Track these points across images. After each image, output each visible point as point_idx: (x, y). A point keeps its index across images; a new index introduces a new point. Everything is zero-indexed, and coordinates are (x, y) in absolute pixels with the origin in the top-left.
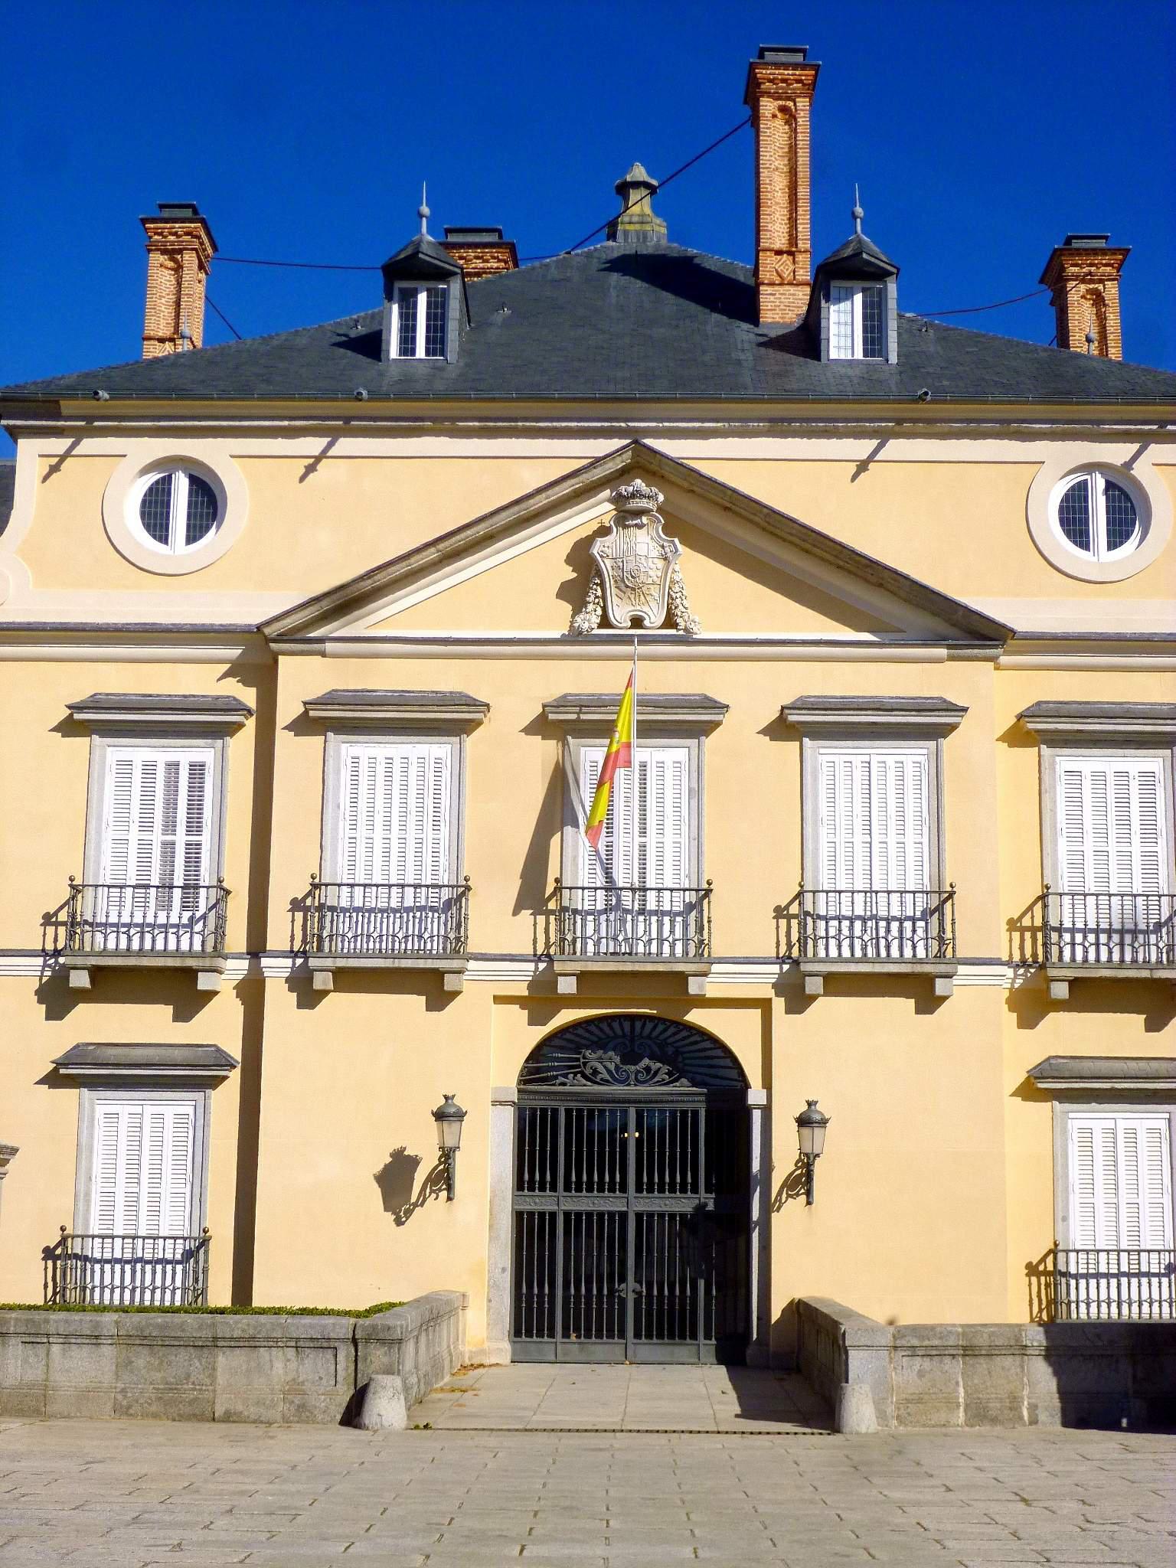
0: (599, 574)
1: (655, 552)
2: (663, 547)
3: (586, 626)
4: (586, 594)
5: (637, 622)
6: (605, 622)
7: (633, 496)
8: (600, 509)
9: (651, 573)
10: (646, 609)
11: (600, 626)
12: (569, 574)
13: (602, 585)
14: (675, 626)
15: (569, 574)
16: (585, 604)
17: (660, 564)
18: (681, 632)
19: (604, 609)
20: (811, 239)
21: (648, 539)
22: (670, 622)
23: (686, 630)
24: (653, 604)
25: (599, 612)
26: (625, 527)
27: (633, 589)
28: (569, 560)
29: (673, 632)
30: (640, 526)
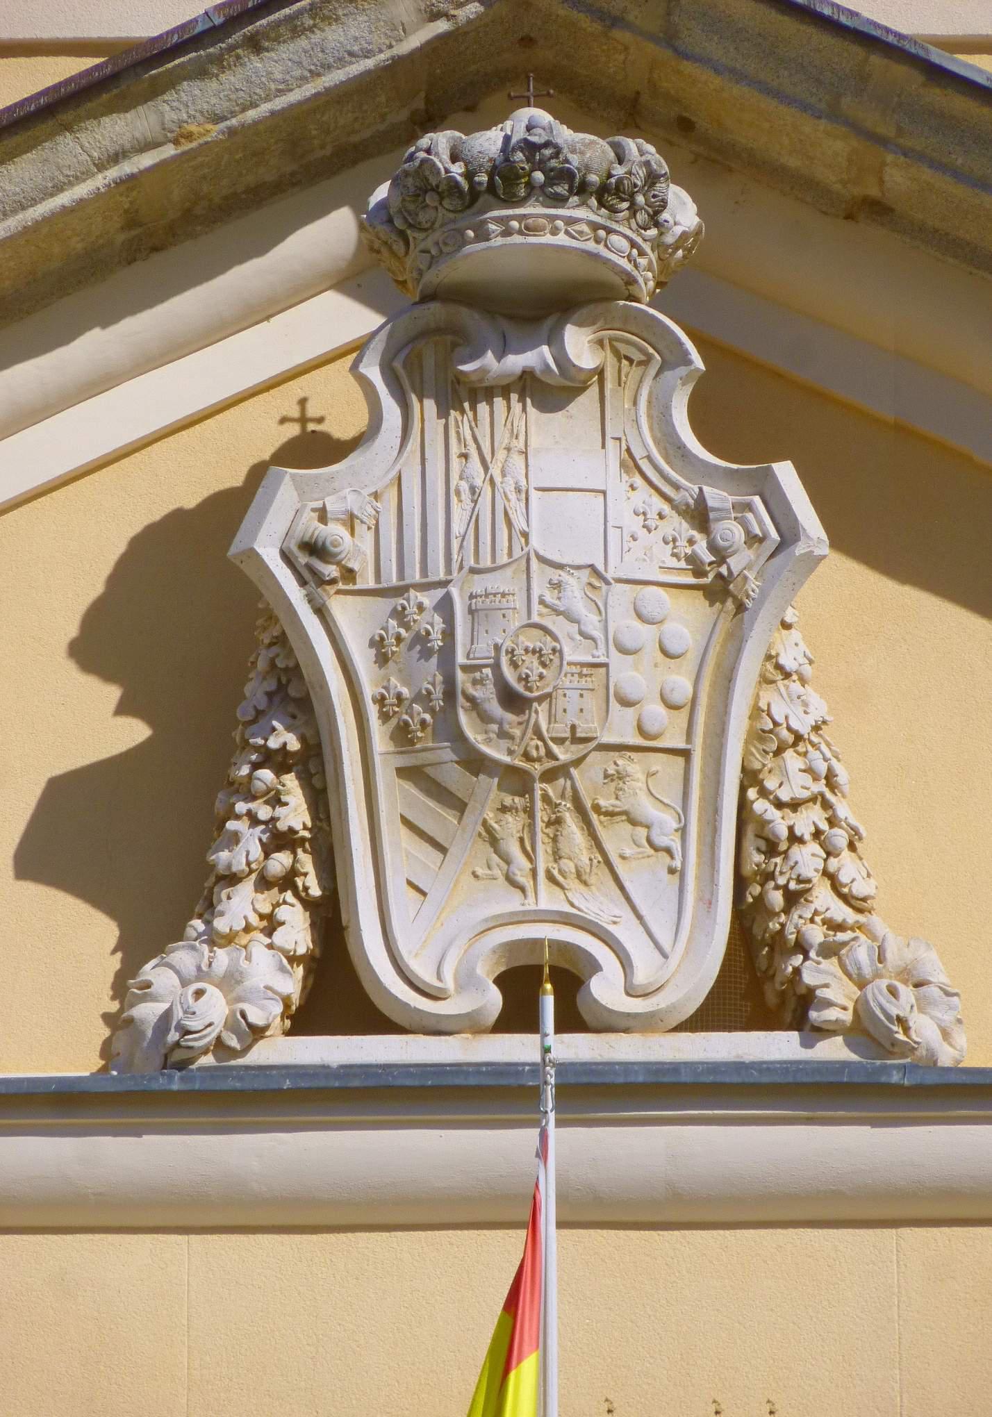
0: (295, 694)
1: (650, 545)
2: (700, 516)
3: (213, 1011)
4: (215, 830)
5: (541, 985)
6: (335, 991)
7: (505, 182)
8: (288, 325)
9: (625, 674)
10: (598, 904)
11: (303, 1021)
12: (97, 726)
13: (314, 766)
14: (795, 1009)
15: (97, 726)
16: (200, 890)
17: (686, 621)
18: (833, 1050)
19: (330, 918)
20: (135, 107)
21: (604, 468)
22: (756, 984)
23: (867, 1031)
24: (644, 878)
25: (297, 931)
26: (458, 394)
27: (516, 781)
28: (101, 644)
29: (780, 1046)
30: (548, 391)
